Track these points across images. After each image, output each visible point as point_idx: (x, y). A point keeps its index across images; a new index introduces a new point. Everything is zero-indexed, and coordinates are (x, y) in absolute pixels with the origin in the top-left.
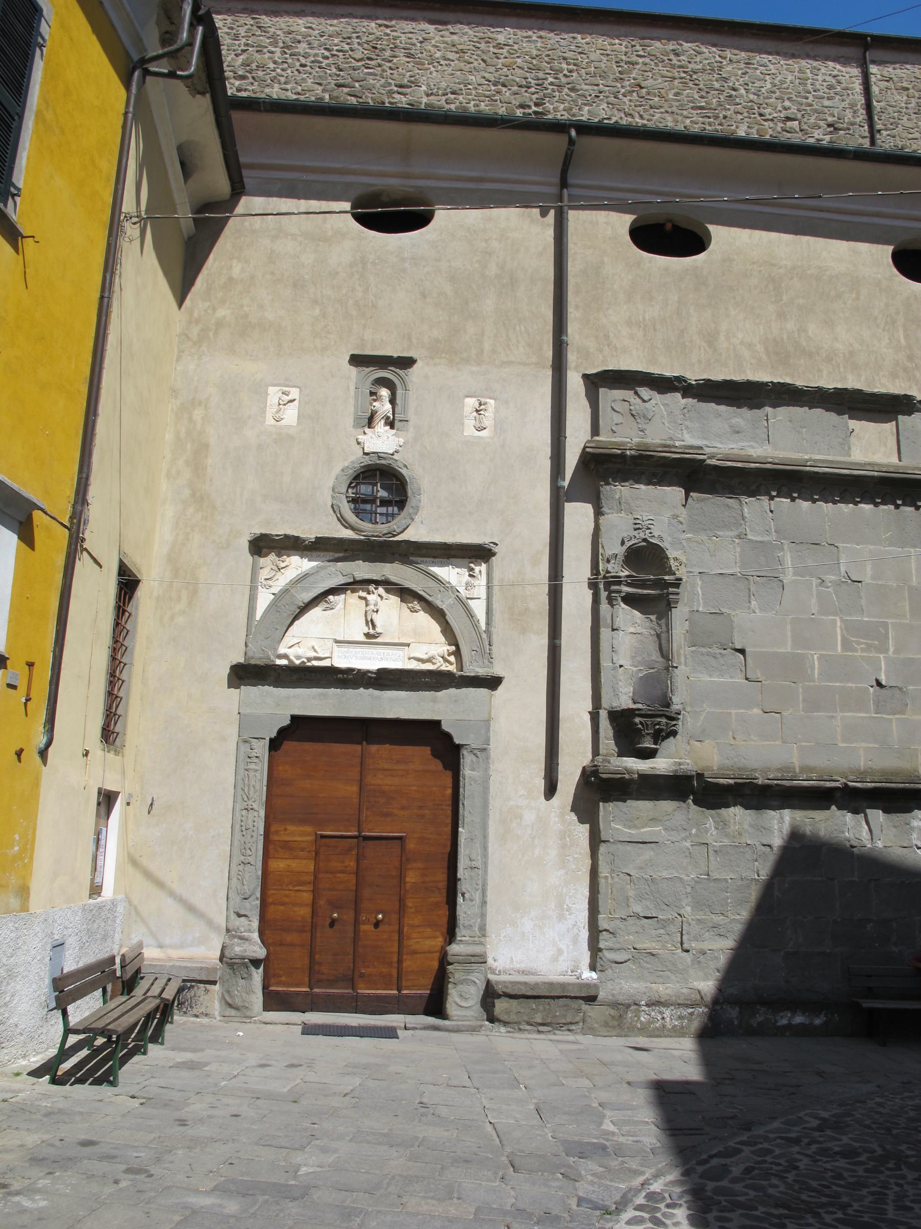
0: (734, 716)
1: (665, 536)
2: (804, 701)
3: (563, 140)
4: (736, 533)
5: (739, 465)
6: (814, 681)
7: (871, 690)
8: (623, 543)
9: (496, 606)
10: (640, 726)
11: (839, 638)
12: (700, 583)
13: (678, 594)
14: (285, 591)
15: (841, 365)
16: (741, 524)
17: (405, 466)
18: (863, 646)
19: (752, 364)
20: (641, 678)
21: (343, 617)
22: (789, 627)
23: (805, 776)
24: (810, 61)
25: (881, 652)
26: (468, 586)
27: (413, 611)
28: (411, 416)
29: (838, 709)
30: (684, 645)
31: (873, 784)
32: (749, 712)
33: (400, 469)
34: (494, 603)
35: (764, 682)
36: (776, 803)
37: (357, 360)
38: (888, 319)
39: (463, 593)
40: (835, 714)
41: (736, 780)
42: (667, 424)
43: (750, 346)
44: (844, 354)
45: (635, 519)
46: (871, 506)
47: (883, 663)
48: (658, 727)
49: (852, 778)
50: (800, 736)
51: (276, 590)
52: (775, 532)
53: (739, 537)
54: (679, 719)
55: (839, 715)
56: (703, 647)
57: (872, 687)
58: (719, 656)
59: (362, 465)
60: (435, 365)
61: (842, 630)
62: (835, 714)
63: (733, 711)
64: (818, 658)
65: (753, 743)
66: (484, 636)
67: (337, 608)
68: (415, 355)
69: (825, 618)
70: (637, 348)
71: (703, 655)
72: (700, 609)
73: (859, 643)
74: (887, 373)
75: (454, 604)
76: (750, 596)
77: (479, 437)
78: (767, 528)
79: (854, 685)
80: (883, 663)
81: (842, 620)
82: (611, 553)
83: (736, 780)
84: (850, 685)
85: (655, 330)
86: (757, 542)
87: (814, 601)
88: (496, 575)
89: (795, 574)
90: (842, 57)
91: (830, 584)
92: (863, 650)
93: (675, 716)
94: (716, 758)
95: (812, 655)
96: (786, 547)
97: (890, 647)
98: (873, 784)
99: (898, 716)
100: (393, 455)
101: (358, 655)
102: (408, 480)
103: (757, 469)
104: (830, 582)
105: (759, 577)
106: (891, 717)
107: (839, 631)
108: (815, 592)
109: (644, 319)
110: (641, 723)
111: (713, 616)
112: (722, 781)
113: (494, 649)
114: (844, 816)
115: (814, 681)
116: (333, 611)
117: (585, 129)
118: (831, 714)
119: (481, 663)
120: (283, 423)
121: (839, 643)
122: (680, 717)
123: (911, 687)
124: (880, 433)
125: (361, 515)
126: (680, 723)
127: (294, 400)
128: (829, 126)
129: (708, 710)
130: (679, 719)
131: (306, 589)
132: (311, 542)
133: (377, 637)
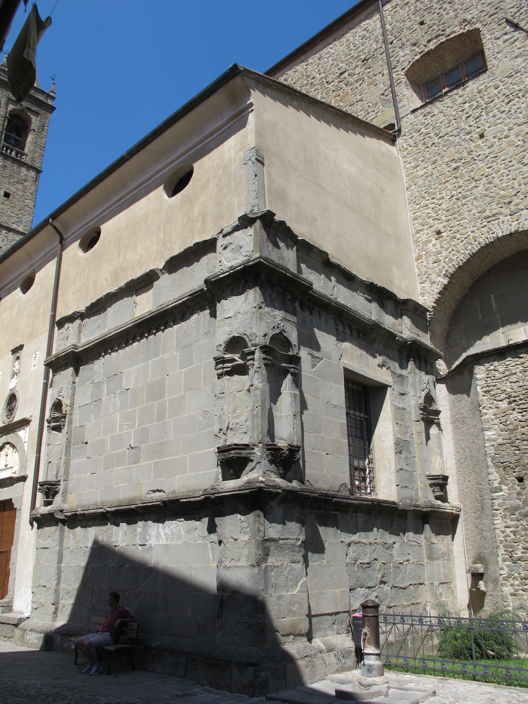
3: (49, 227)
5: (87, 346)
7: (128, 451)
24: (351, 32)
31: (115, 508)
36: (91, 523)
46: (138, 342)
54: (60, 484)
68: (22, 344)
90: (369, 14)
98: (115, 508)
103: (93, 345)
114: (113, 528)
117: (55, 216)
128: (363, 61)
130: (60, 484)
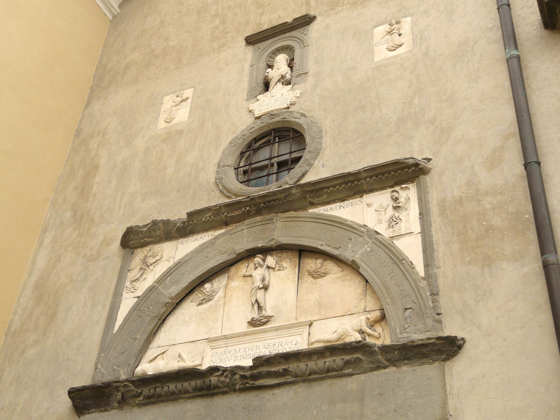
9: (437, 236)
14: (151, 290)
17: (303, 115)
21: (222, 308)
26: (393, 222)
27: (316, 275)
28: (311, 67)
33: (297, 120)
34: (433, 233)
37: (251, 41)
39: (385, 231)
51: (139, 293)
59: (252, 130)
60: (336, 14)
66: (424, 284)
67: (216, 298)
75: (372, 251)
77: (395, 57)
88: (434, 197)
100: (288, 108)
101: (239, 354)
102: (305, 127)
113: (443, 300)
116: (210, 303)
119: (421, 326)
120: (174, 122)
125: (370, 337)
127: (187, 98)
131: (173, 283)
132: (184, 223)
133: (265, 323)
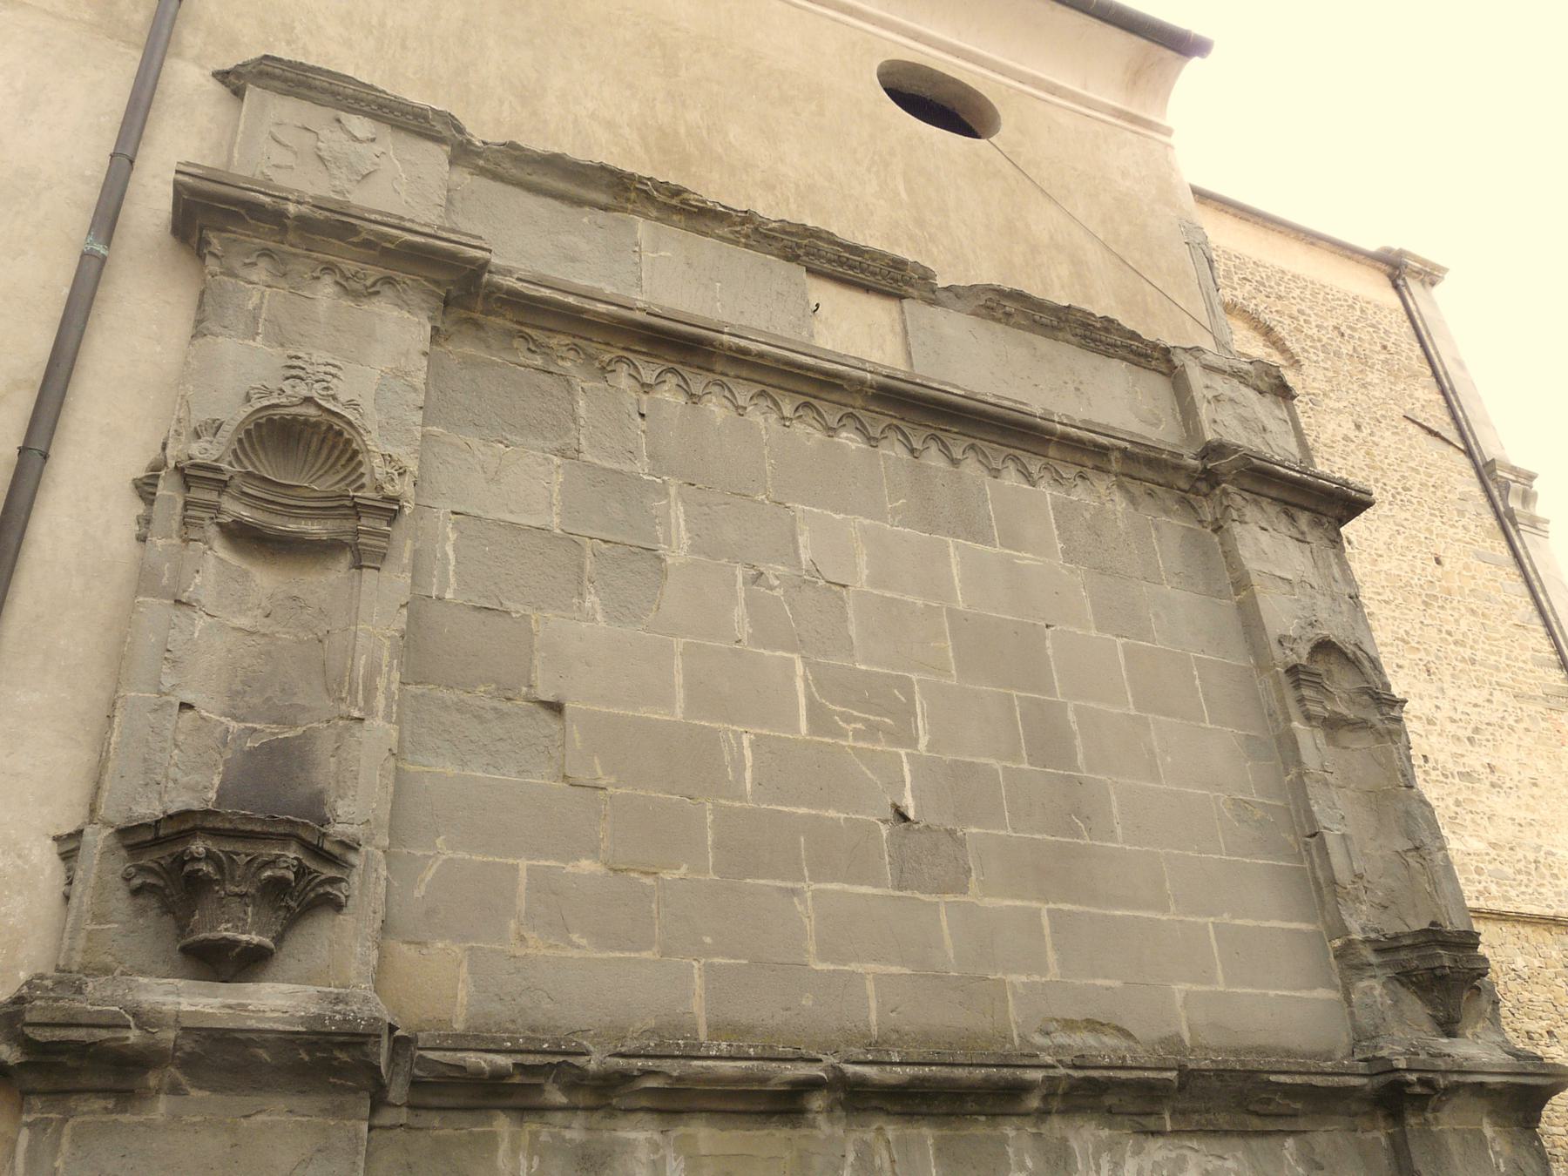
0: (523, 874)
1: (367, 405)
2: (718, 845)
4: (556, 444)
5: (571, 300)
6: (741, 798)
8: (248, 399)
10: (205, 868)
11: (802, 701)
12: (452, 536)
13: (387, 536)
15: (792, 200)
16: (570, 430)
18: (859, 726)
19: (611, 153)
20: (252, 753)
22: (678, 663)
23: (724, 1045)
25: (901, 744)
29: (806, 873)
30: (390, 666)
32: (569, 868)
35: (611, 790)
38: (876, 158)
40: (798, 885)
41: (519, 1058)
42: (403, 194)
43: (610, 125)
44: (797, 186)
45: (291, 357)
47: (906, 768)
48: (268, 873)
49: (856, 1052)
50: (708, 940)
52: (650, 456)
53: (561, 453)
55: (809, 887)
56: (449, 687)
57: (885, 821)
58: (490, 715)
61: (807, 686)
62: (798, 885)
63: (523, 863)
64: (751, 743)
65: (575, 953)
69: (767, 653)
70: (357, 65)
71: (446, 707)
72: (449, 596)
73: (849, 719)
74: (878, 234)
76: (580, 583)
78: (631, 446)
79: (843, 816)
80: (906, 768)
81: (807, 663)
82: (205, 417)
83: (519, 1058)
84: (832, 813)
85: (404, 47)
86: (604, 469)
87: (739, 611)
89: (694, 549)
91: (777, 583)
92: (858, 735)
93: (336, 850)
94: (462, 995)
95: (738, 736)
96: (673, 491)
97: (921, 732)
99: (950, 898)
104: (777, 577)
105: (605, 542)
106: (933, 898)
107: (800, 685)
108: (742, 595)
109: (382, 24)
110: (210, 856)
111: (482, 615)
112: (472, 1059)
115: (741, 798)
118: (790, 885)
121: (803, 712)
122: (352, 858)
123: (974, 830)
124: (869, 326)
126: (355, 879)
129: (450, 854)
